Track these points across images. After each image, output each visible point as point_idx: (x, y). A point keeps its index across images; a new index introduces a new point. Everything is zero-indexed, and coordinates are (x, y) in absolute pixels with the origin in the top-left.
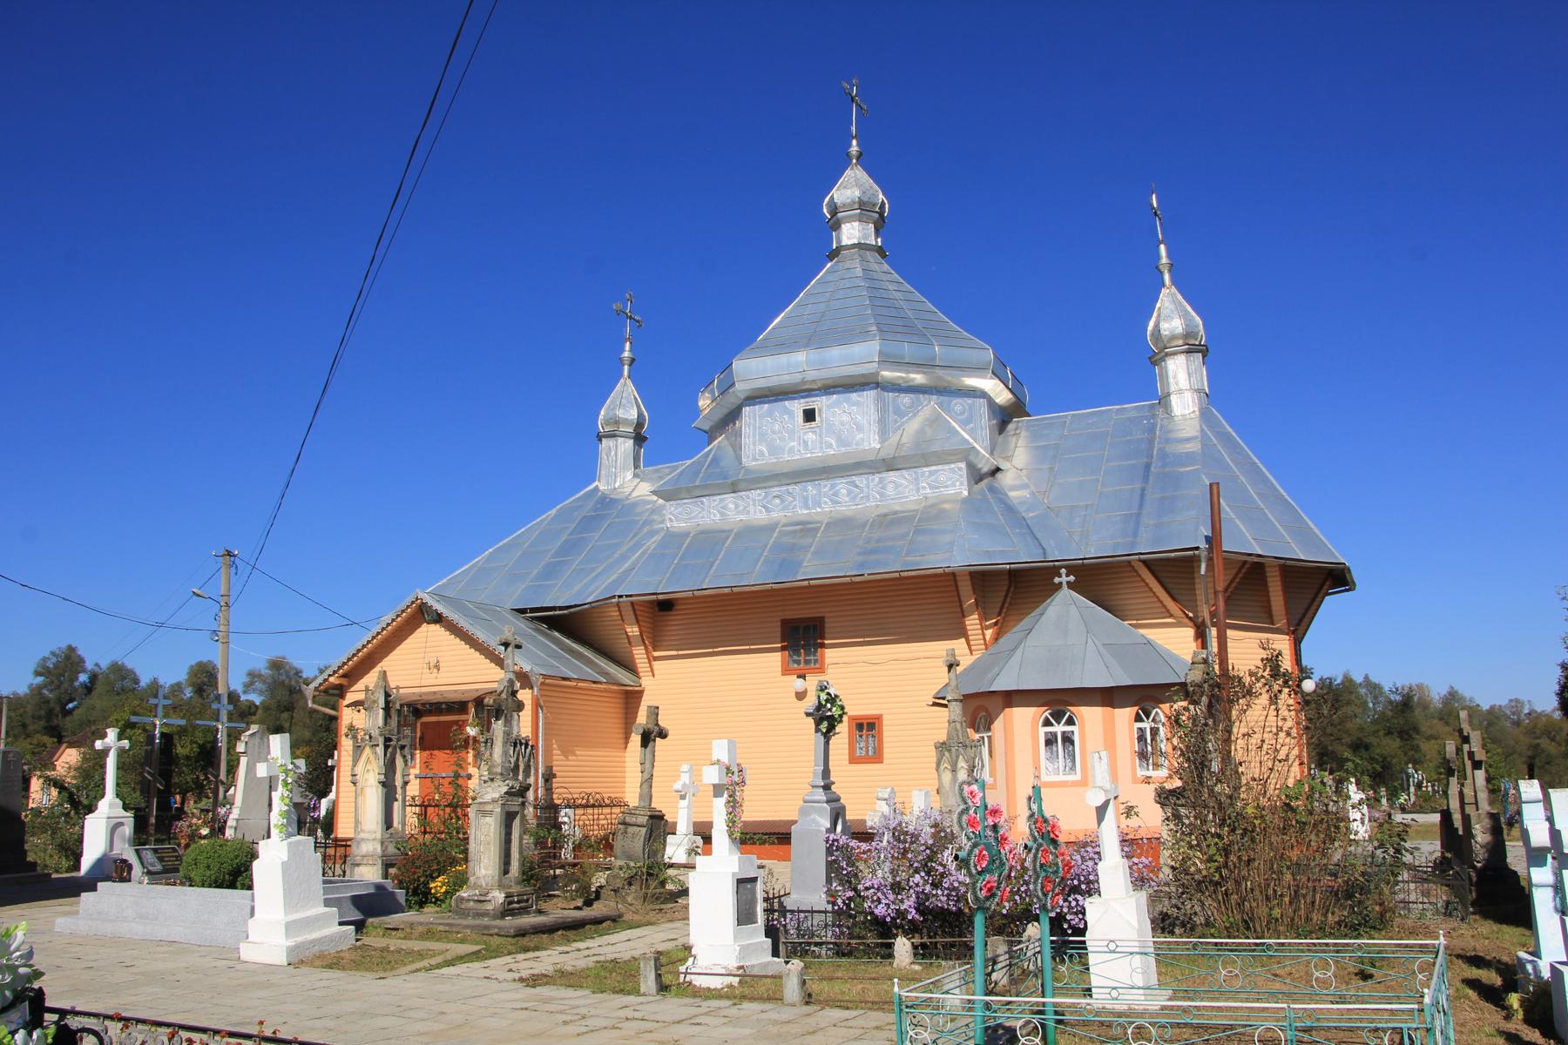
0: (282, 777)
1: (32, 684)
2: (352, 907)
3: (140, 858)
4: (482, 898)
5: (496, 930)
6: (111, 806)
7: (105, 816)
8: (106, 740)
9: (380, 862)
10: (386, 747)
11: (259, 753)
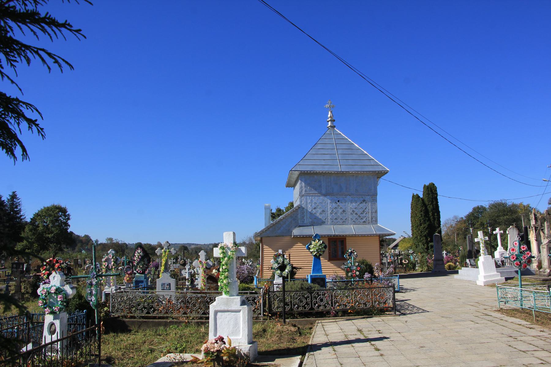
0: (481, 241)
1: (548, 208)
2: (516, 273)
3: (470, 262)
4: (544, 271)
5: (538, 279)
6: (500, 249)
7: (499, 251)
8: (496, 231)
9: (537, 262)
10: (536, 230)
11: (513, 233)
